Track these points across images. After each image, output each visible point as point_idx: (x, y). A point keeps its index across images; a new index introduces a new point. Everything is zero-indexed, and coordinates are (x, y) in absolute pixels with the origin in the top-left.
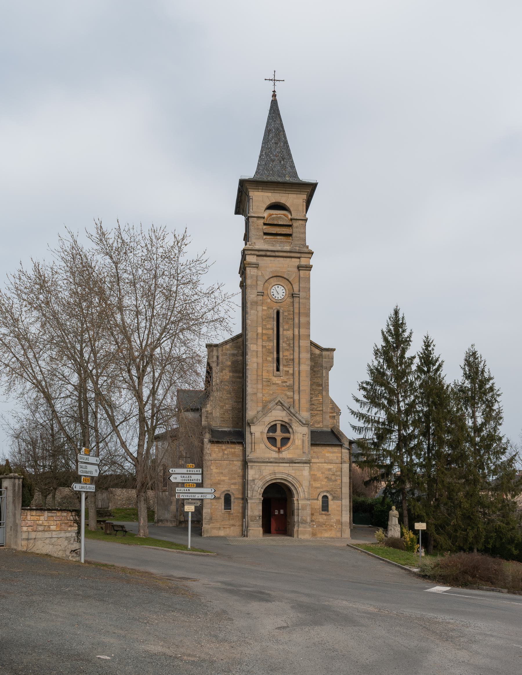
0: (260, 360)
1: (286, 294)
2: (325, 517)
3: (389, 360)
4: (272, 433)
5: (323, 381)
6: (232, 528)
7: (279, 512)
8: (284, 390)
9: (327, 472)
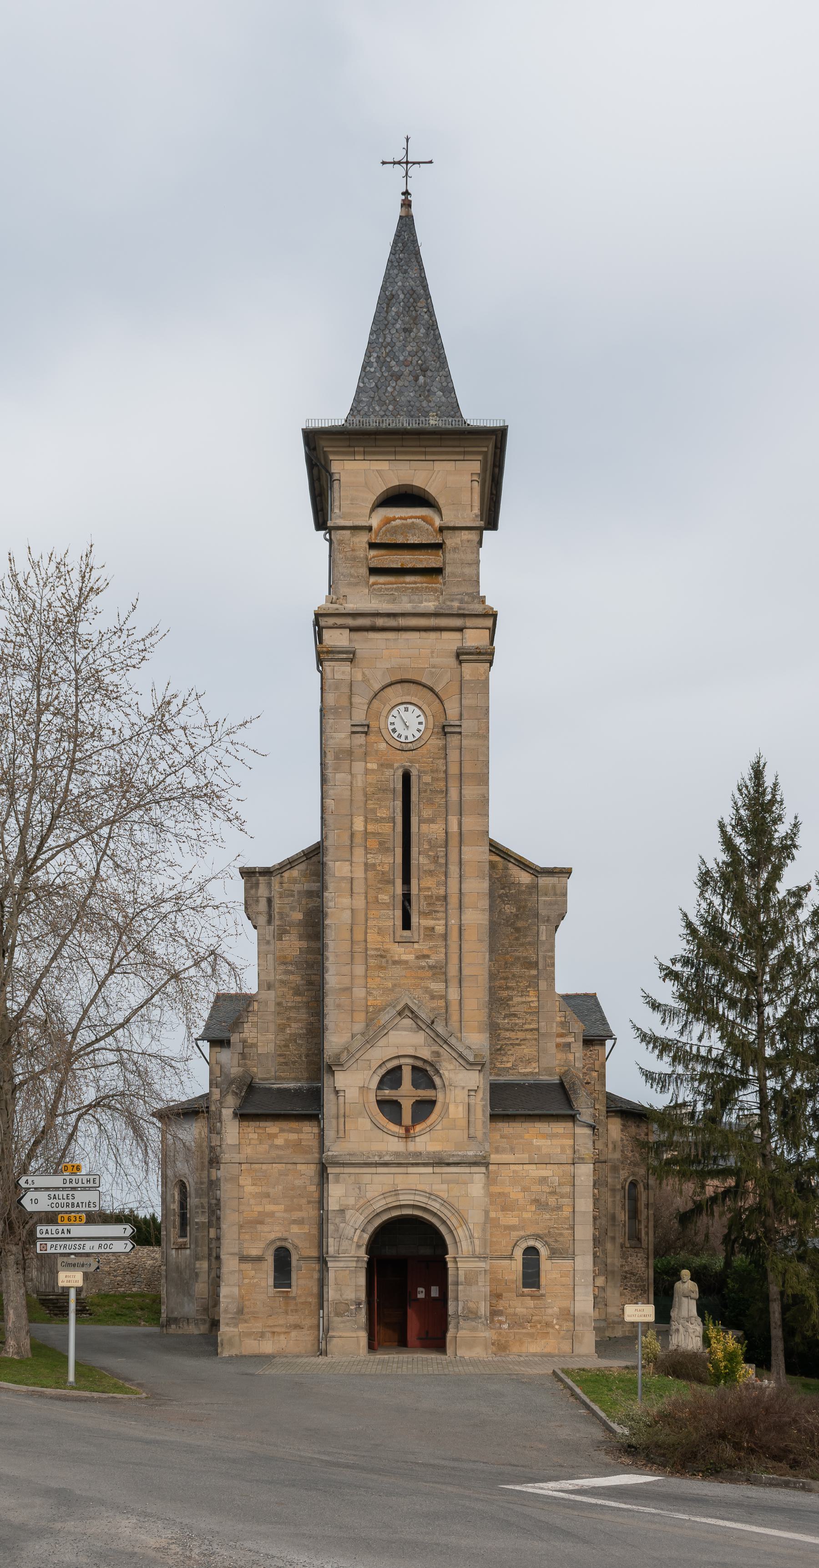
0: (360, 902)
1: (426, 728)
2: (530, 1303)
3: (739, 900)
4: (392, 1088)
5: (540, 954)
6: (293, 1334)
7: (428, 1292)
8: (422, 979)
9: (535, 1188)
